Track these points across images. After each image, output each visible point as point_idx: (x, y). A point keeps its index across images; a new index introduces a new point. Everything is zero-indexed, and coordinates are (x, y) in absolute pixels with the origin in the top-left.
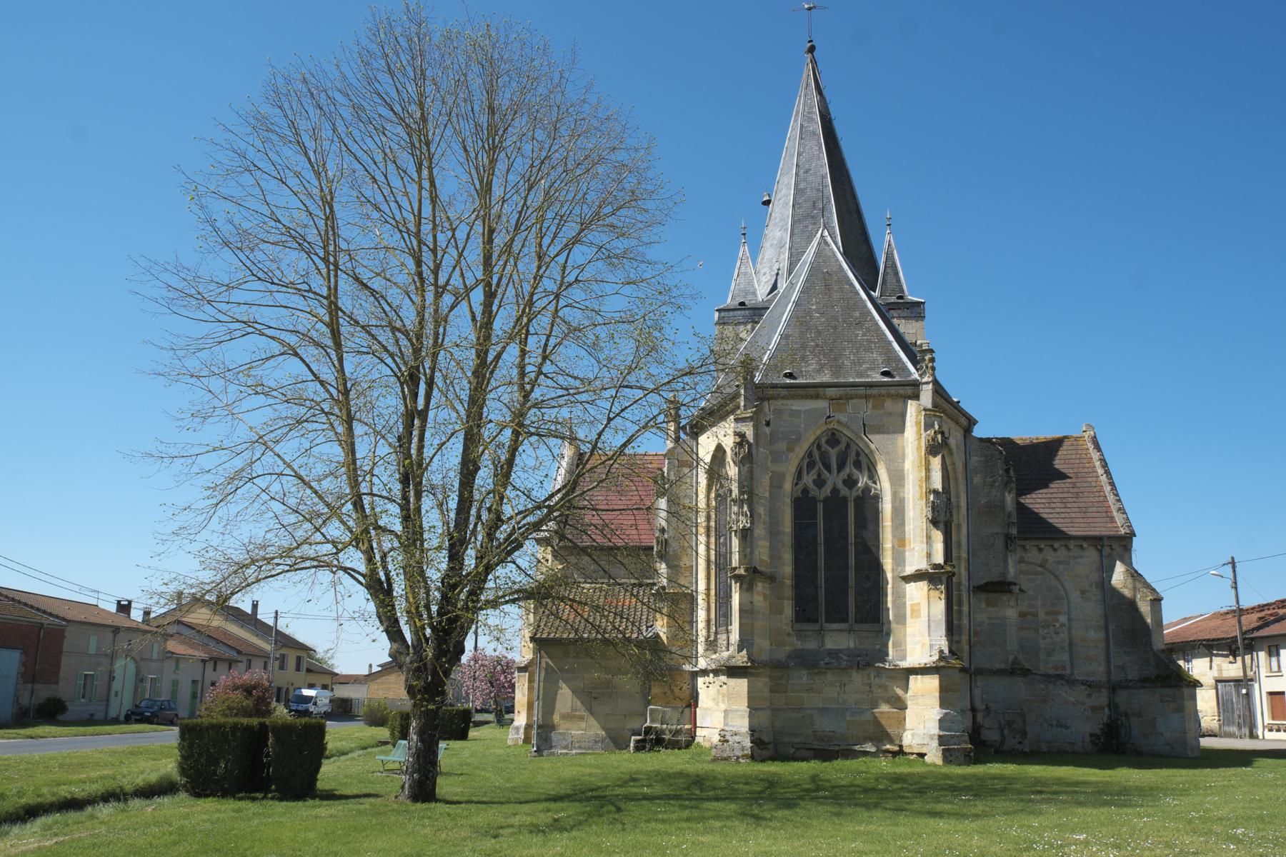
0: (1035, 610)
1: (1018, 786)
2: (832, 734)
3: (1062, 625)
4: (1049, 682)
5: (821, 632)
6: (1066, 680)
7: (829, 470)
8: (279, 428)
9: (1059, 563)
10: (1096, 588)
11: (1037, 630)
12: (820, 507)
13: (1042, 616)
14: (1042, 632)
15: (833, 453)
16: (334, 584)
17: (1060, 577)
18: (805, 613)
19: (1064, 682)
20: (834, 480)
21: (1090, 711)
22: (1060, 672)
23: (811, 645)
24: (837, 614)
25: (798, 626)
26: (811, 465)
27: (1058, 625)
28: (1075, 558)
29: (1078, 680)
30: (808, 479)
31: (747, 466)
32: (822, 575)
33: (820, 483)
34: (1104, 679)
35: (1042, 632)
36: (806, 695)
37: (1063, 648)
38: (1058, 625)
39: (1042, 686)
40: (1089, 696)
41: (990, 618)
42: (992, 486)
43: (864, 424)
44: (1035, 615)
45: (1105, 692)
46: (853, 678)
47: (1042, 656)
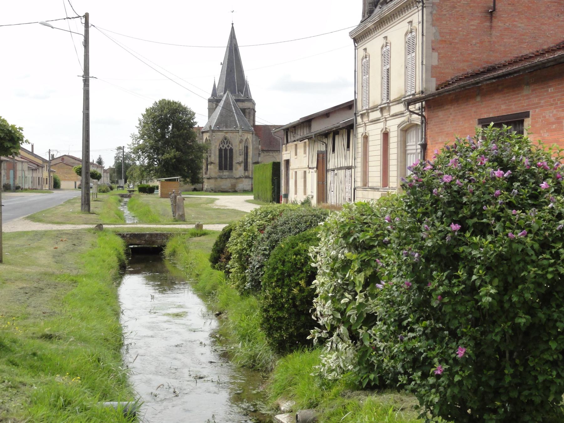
1: (456, 41)
5: (223, 172)
7: (225, 144)
8: (323, 157)
15: (225, 141)
16: (249, 185)
20: (226, 146)
23: (221, 174)
24: (226, 169)
26: (222, 143)
30: (221, 146)
32: (223, 162)
33: (223, 146)
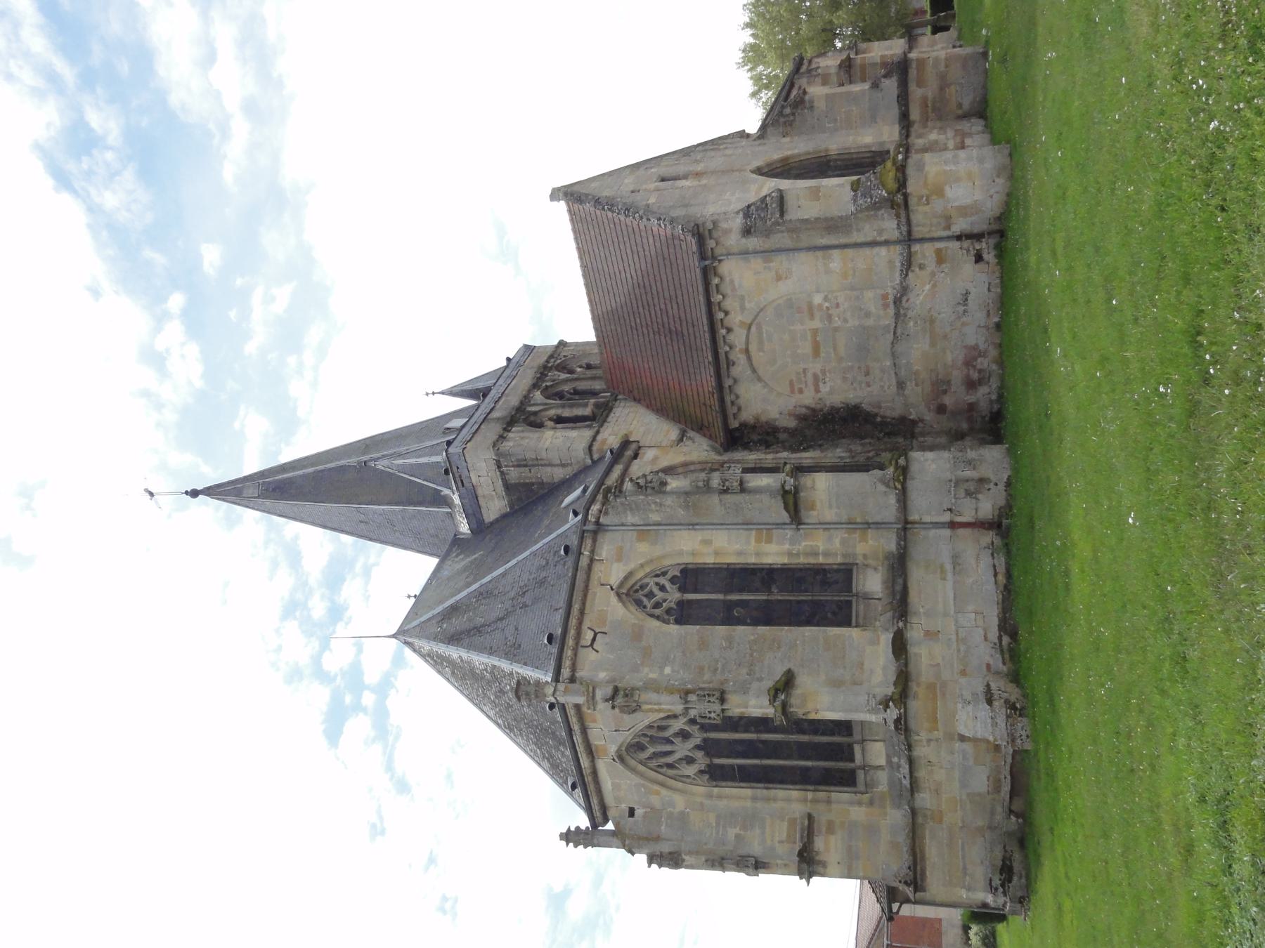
0: (808, 332)
2: (991, 778)
3: (826, 299)
4: (905, 315)
6: (902, 296)
9: (743, 308)
10: (772, 261)
11: (836, 330)
12: (717, 761)
13: (817, 324)
14: (837, 322)
17: (762, 306)
18: (846, 779)
19: (904, 299)
21: (944, 266)
22: (891, 300)
24: (845, 753)
25: (861, 787)
27: (827, 304)
28: (734, 289)
29: (901, 283)
31: (684, 857)
34: (898, 249)
35: (837, 322)
36: (944, 796)
37: (857, 298)
38: (827, 304)
39: (911, 324)
40: (921, 267)
41: (830, 507)
42: (661, 505)
43: (616, 731)
44: (815, 332)
45: (916, 248)
46: (922, 755)
47: (870, 322)
